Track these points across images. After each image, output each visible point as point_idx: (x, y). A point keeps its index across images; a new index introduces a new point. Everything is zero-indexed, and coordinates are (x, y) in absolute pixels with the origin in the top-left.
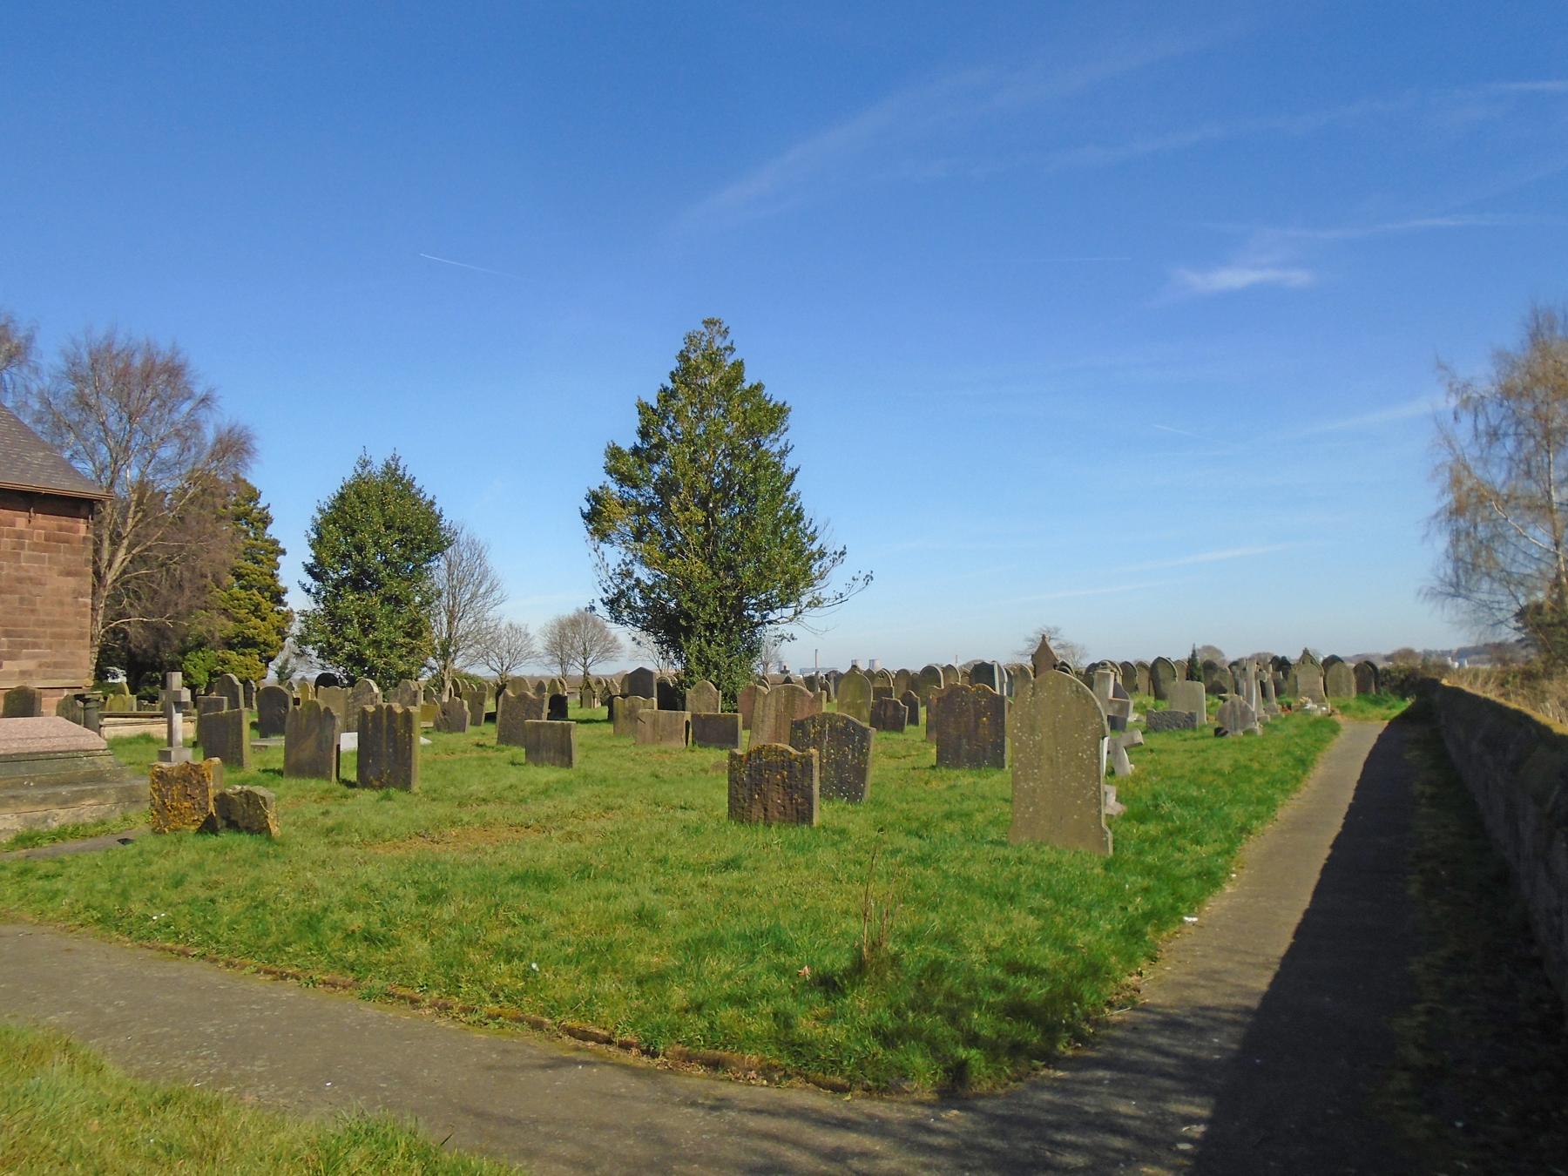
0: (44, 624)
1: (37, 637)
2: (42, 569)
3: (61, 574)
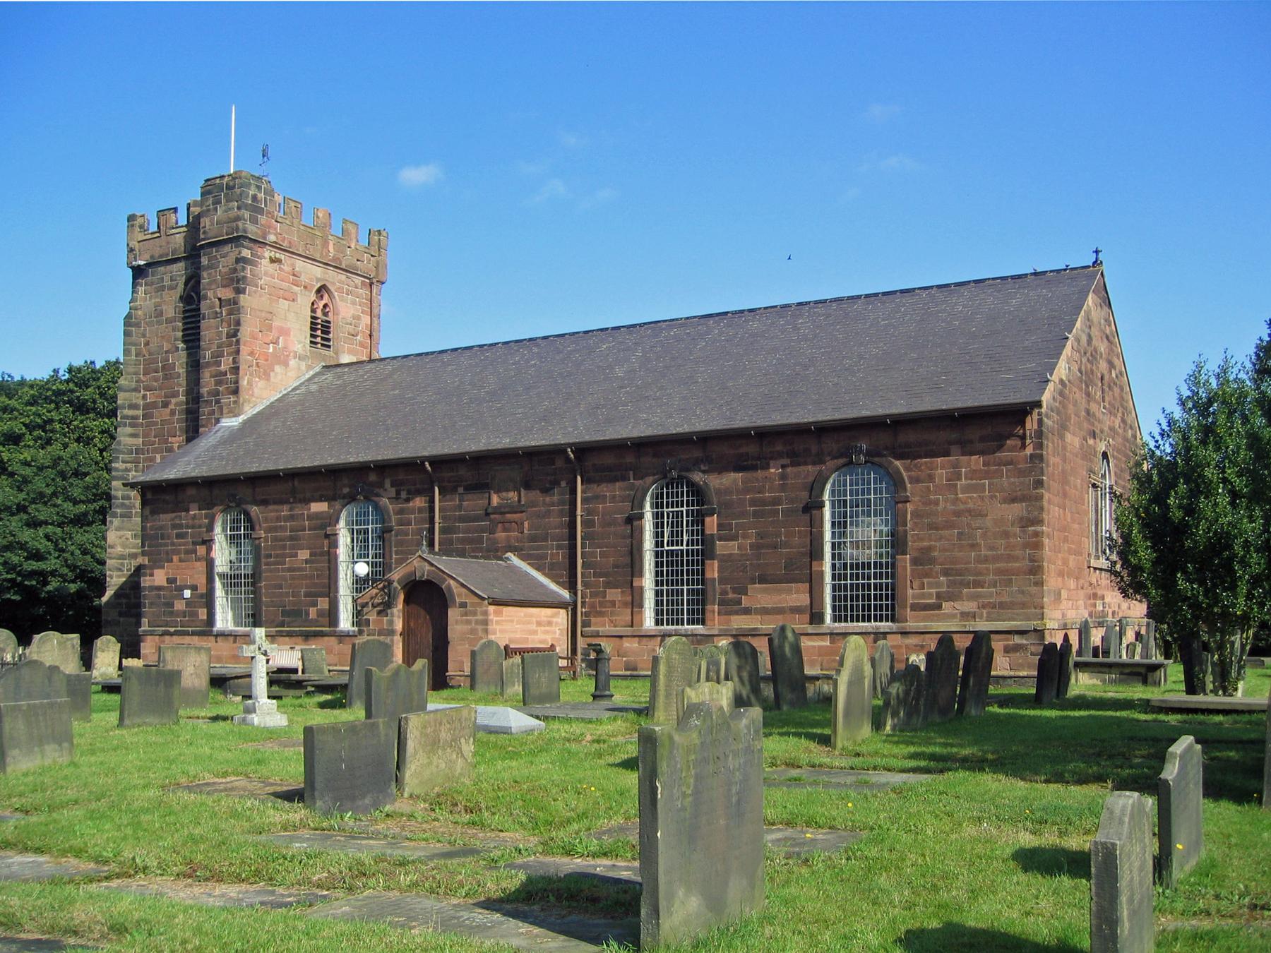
0: (986, 560)
1: (980, 574)
2: (982, 498)
3: (1005, 501)
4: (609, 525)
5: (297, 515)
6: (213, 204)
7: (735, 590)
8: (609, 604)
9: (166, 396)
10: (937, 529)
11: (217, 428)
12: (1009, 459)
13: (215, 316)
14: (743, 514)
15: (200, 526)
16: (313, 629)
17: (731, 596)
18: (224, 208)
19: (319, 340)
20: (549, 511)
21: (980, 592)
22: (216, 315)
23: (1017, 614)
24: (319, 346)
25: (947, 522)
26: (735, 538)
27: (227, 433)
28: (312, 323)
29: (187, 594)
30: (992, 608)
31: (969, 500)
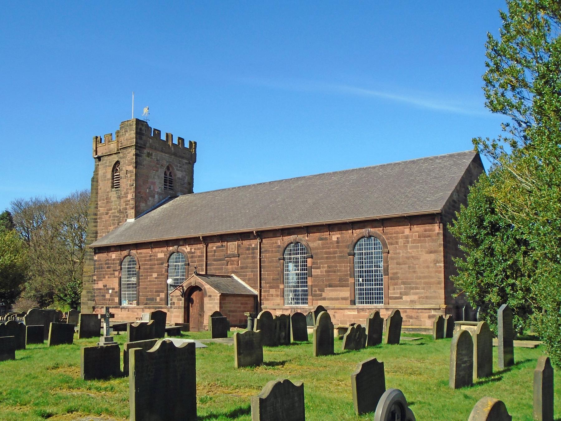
2: (418, 252)
4: (271, 262)
5: (153, 259)
6: (124, 132)
7: (319, 290)
8: (271, 296)
9: (107, 210)
10: (400, 264)
11: (125, 223)
12: (429, 235)
13: (125, 177)
14: (322, 258)
15: (116, 264)
16: (158, 306)
17: (318, 292)
18: (129, 134)
19: (168, 187)
20: (248, 257)
21: (417, 292)
22: (126, 177)
23: (434, 302)
24: (168, 189)
25: (404, 262)
26: (319, 268)
27: (129, 225)
28: (165, 180)
29: (110, 291)
30: (423, 299)
31: (413, 252)
